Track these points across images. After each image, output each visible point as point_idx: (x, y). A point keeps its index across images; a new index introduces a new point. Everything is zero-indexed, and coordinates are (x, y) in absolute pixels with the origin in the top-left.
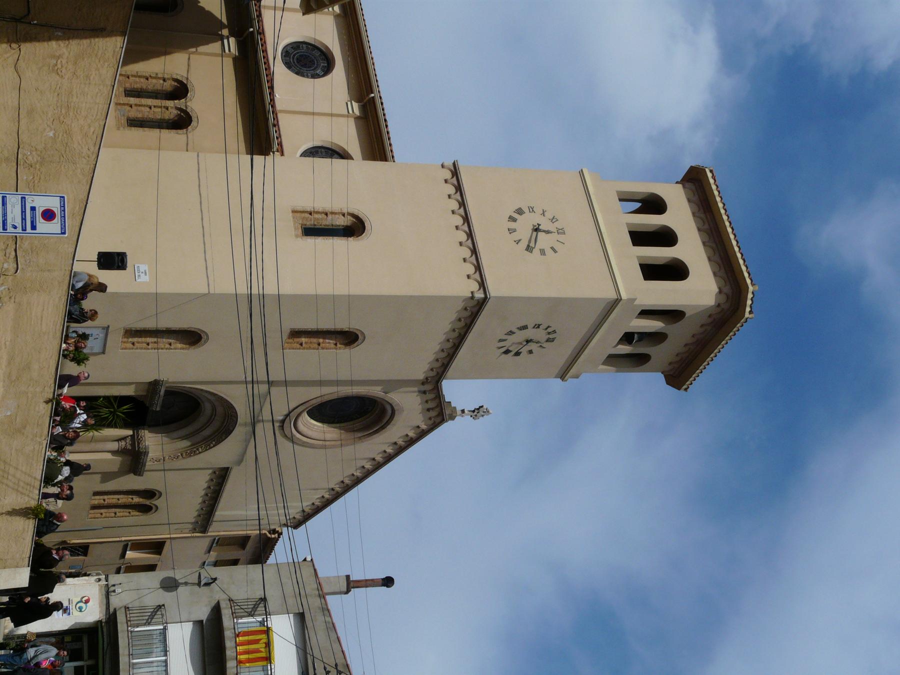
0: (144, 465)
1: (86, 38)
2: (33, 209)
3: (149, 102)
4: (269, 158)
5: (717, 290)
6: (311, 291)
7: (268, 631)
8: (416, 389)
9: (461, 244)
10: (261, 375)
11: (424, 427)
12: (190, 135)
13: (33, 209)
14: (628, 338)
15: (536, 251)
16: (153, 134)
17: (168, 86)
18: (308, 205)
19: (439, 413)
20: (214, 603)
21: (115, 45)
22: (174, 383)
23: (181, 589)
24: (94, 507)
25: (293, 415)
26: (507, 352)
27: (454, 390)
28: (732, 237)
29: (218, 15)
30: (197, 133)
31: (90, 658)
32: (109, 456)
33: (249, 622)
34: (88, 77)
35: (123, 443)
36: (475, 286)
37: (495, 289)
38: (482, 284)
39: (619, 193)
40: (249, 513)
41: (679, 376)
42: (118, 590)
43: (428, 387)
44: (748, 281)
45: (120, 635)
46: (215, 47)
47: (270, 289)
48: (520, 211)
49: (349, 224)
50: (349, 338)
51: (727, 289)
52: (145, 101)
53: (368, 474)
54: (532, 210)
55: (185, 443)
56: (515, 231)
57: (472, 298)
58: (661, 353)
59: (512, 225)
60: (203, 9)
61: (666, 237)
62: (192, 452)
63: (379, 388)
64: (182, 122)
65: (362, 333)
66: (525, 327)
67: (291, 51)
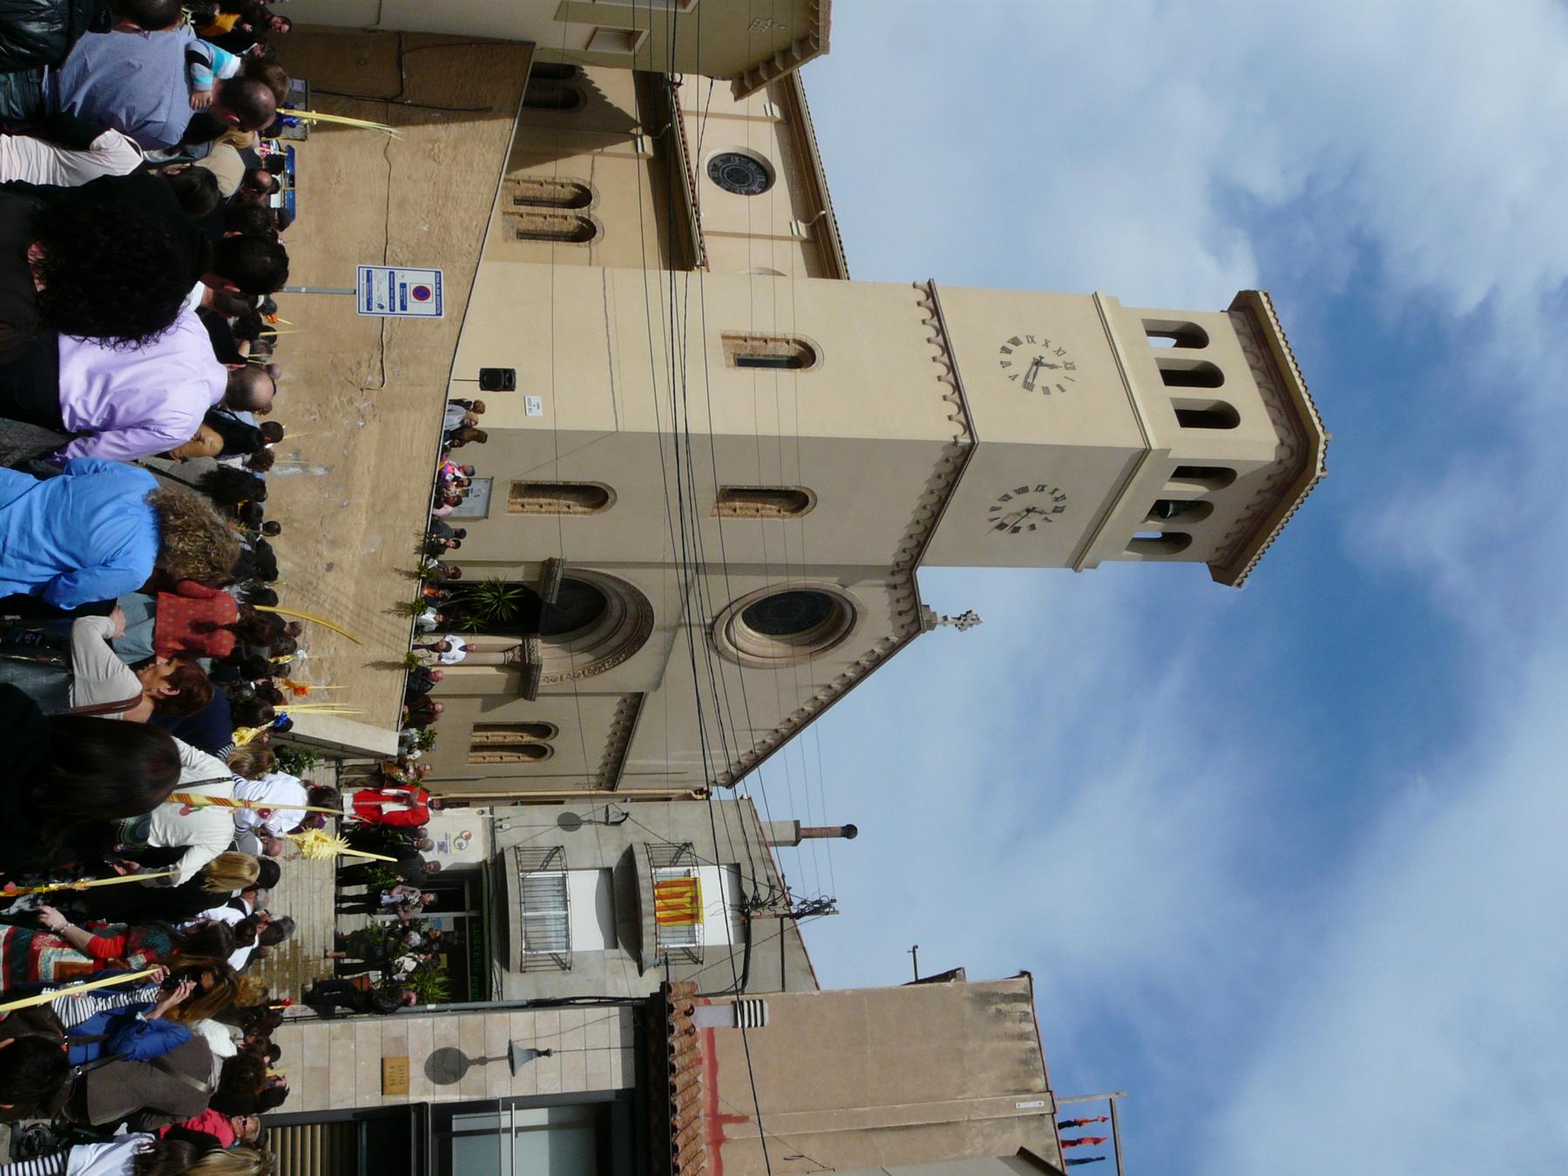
0: (536, 684)
1: (469, 120)
2: (403, 286)
4: (695, 274)
5: (1278, 441)
6: (749, 430)
7: (695, 882)
10: (701, 119)
11: (894, 639)
12: (594, 248)
13: (403, 286)
14: (1160, 509)
16: (545, 247)
17: (567, 193)
18: (744, 330)
19: (914, 619)
20: (626, 847)
21: (498, 133)
22: (573, 563)
23: (583, 827)
24: (476, 748)
25: (726, 616)
26: (1001, 526)
27: (933, 582)
28: (1296, 374)
30: (600, 245)
32: (493, 671)
34: (470, 163)
35: (510, 654)
36: (959, 430)
37: (983, 434)
38: (968, 427)
41: (1227, 568)
42: (506, 825)
43: (900, 579)
44: (1319, 428)
46: (626, 147)
47: (698, 427)
48: (1016, 342)
50: (796, 501)
51: (1291, 440)
52: (537, 210)
54: (1031, 340)
55: (586, 658)
56: (1009, 364)
57: (955, 443)
58: (1207, 534)
60: (610, 105)
61: (1209, 376)
62: (597, 669)
64: (585, 233)
65: (814, 495)
66: (1024, 490)
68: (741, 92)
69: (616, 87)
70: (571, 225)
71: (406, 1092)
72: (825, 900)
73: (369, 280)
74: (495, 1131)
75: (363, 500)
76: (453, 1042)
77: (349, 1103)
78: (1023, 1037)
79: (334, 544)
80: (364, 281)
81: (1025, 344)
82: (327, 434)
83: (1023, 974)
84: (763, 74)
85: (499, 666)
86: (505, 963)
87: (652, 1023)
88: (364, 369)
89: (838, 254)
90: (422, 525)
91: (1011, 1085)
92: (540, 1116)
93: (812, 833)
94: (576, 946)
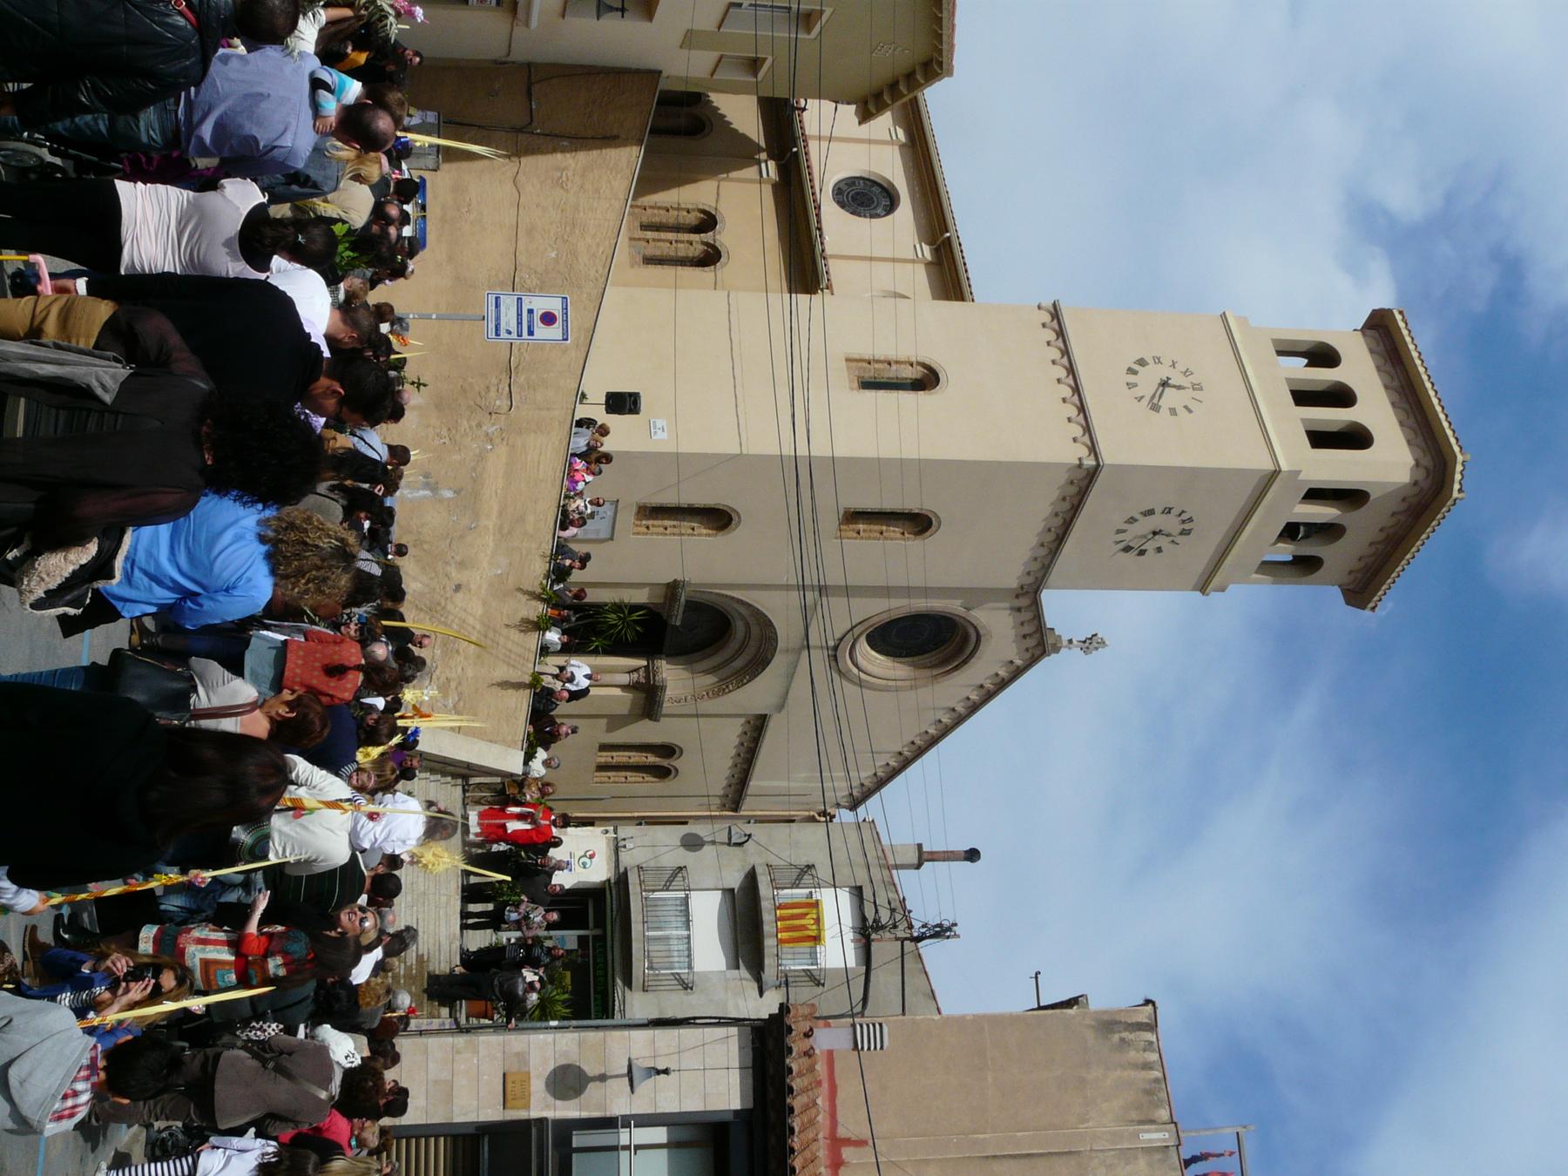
2: (531, 311)
3: (671, 236)
4: (817, 298)
7: (816, 904)
8: (1007, 605)
9: (1064, 400)
10: (824, 144)
11: (1018, 662)
14: (1290, 532)
15: (1164, 410)
16: (668, 272)
17: (693, 219)
19: (1039, 643)
20: (748, 868)
21: (628, 158)
23: (706, 848)
24: (602, 768)
25: (849, 640)
26: (1127, 549)
27: (1058, 606)
29: (754, 137)
30: (724, 270)
31: (596, 926)
32: (618, 692)
33: (789, 895)
34: (597, 191)
35: (635, 675)
36: (1084, 452)
37: (1109, 456)
38: (1093, 449)
39: (1276, 342)
40: (792, 784)
41: (1361, 591)
42: (629, 845)
43: (1024, 602)
44: (1456, 449)
45: (632, 898)
46: (750, 172)
47: (820, 449)
49: (918, 376)
50: (920, 523)
52: (663, 235)
53: (946, 731)
54: (1158, 360)
55: (710, 680)
56: (1136, 385)
57: (1080, 466)
59: (1132, 378)
61: (1341, 396)
62: (720, 690)
63: (959, 602)
64: (710, 257)
66: (1151, 512)
67: (845, 188)
68: (865, 116)
69: (741, 113)
70: (697, 250)
71: (527, 1107)
72: (946, 924)
73: (497, 306)
74: (615, 1148)
75: (490, 522)
76: (573, 1059)
77: (472, 1117)
78: (1147, 1066)
79: (462, 565)
80: (492, 307)
81: (1151, 366)
82: (457, 457)
83: (1148, 1002)
84: (887, 98)
85: (624, 687)
86: (628, 983)
87: (771, 1043)
88: (493, 393)
89: (963, 276)
90: (547, 547)
91: (1134, 1115)
92: (659, 1135)
93: (934, 857)
94: (700, 965)
